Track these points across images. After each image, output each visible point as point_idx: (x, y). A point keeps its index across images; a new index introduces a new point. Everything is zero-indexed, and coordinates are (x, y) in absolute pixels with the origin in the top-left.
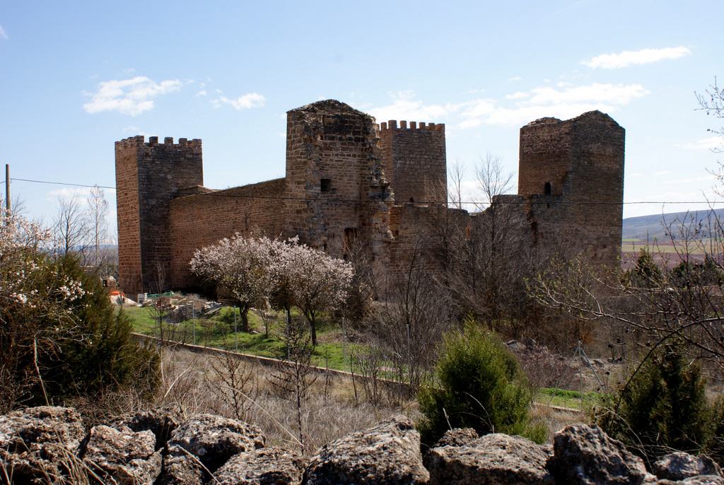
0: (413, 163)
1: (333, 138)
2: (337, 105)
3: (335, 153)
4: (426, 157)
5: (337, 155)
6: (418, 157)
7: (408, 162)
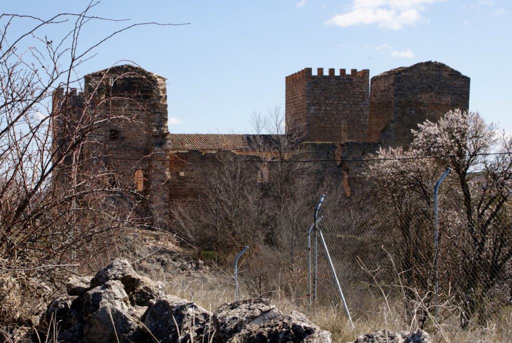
0: (329, 108)
2: (130, 69)
4: (344, 102)
7: (323, 108)
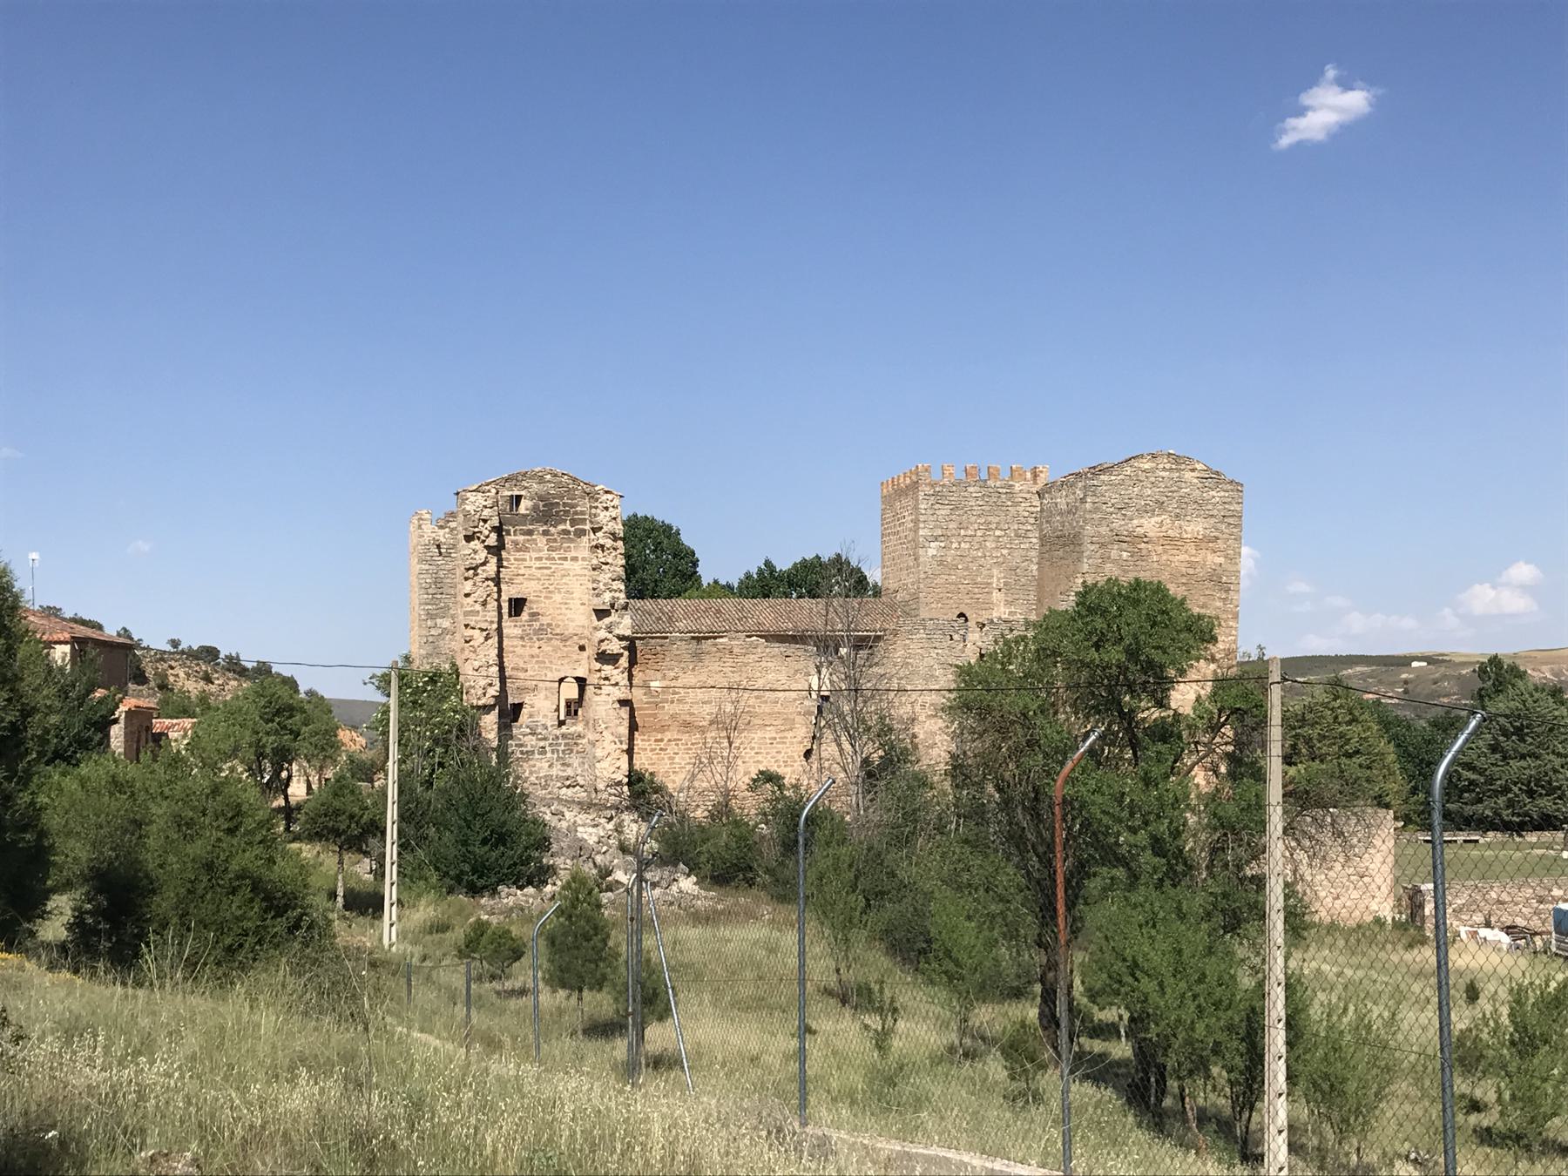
1: (530, 533)
3: (535, 555)
4: (998, 533)
5: (540, 559)
6: (979, 533)
